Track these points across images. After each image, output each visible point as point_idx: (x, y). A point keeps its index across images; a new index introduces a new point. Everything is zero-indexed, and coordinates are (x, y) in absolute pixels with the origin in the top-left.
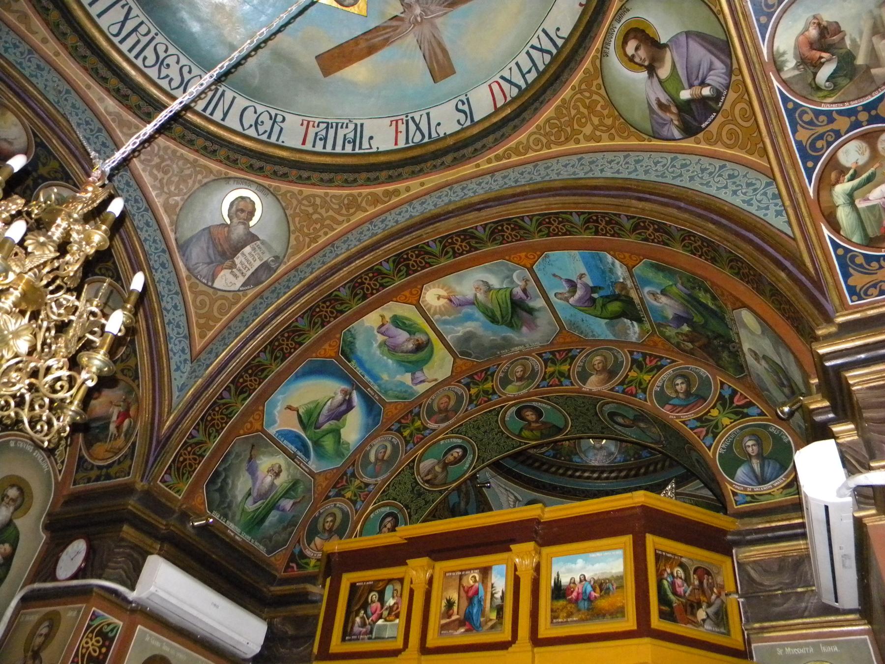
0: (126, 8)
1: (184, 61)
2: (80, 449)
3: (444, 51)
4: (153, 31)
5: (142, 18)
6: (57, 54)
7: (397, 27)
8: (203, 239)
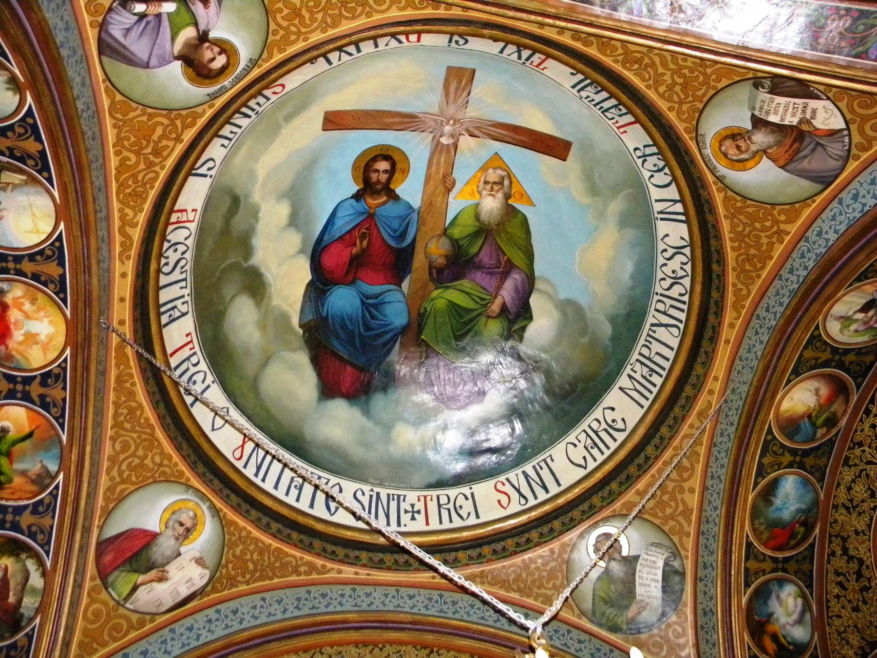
0: (654, 328)
1: (661, 261)
2: (811, 594)
3: (446, 87)
4: (656, 298)
5: (652, 312)
6: (716, 379)
7: (477, 128)
8: (800, 167)
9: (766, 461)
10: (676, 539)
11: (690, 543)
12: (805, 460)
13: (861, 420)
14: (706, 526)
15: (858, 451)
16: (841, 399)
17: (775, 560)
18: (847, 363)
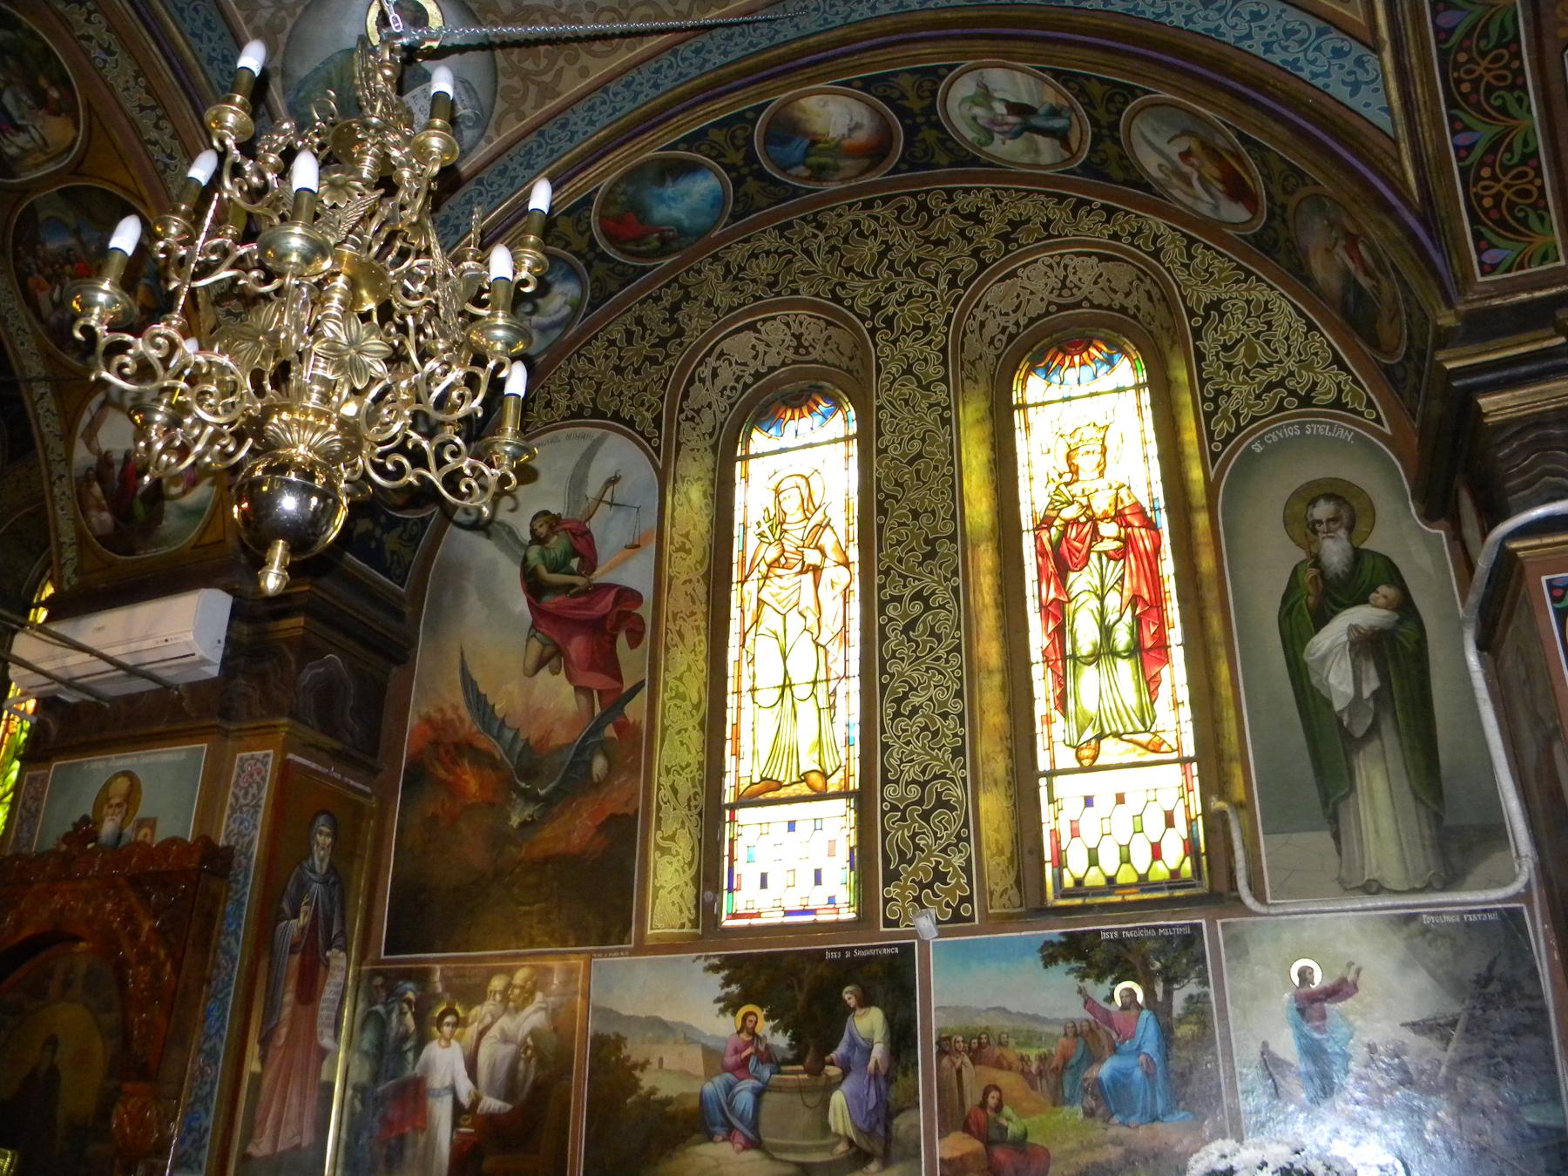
2: (586, 315)
9: (716, 135)
10: (500, 106)
11: (512, 129)
12: (749, 179)
13: (851, 206)
14: (554, 130)
15: (809, 230)
16: (865, 162)
17: (592, 244)
18: (920, 136)
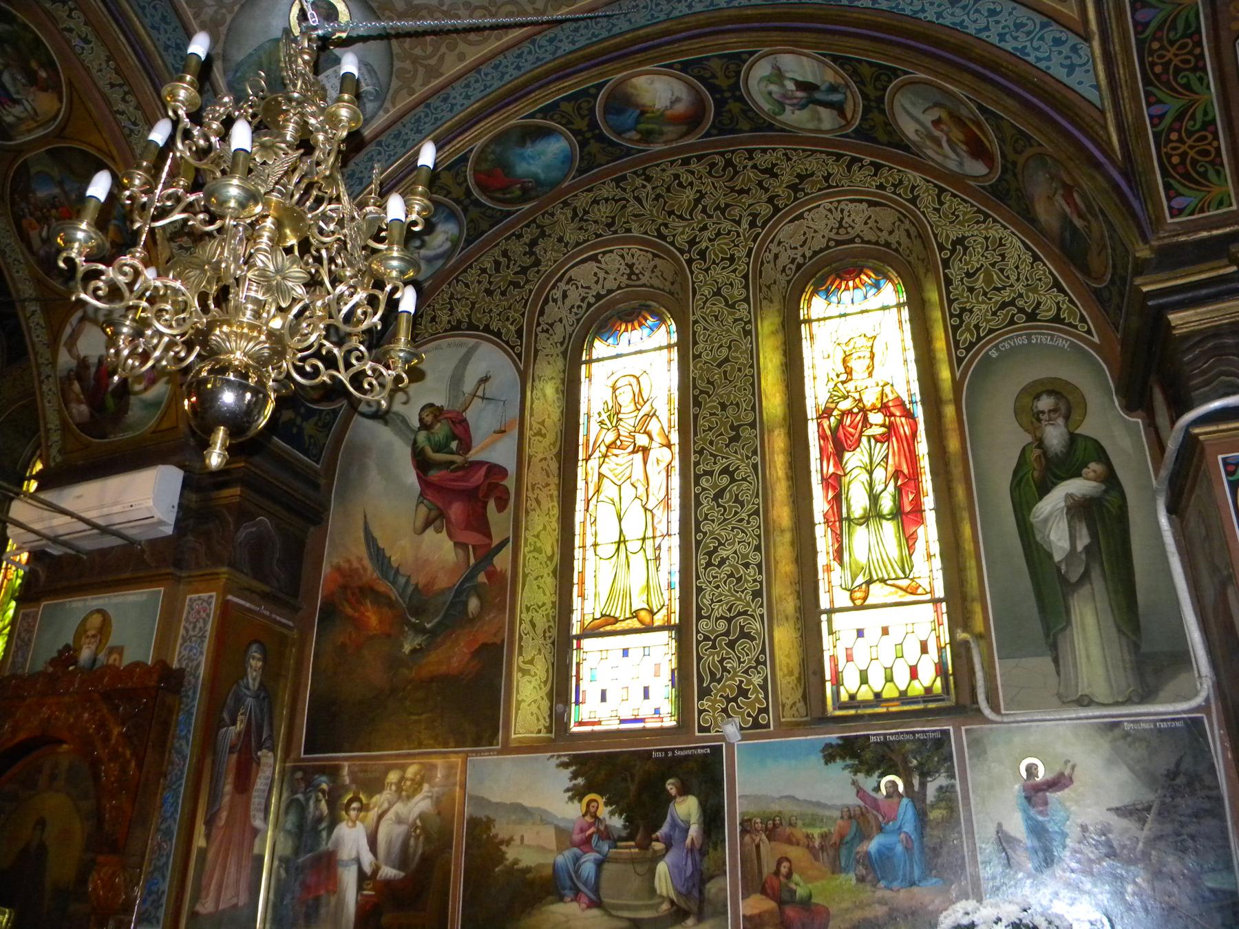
2: (463, 249)
9: (565, 107)
10: (395, 84)
11: (404, 102)
12: (592, 141)
13: (672, 163)
14: (438, 103)
15: (639, 181)
16: (684, 128)
17: (468, 192)
18: (727, 107)
